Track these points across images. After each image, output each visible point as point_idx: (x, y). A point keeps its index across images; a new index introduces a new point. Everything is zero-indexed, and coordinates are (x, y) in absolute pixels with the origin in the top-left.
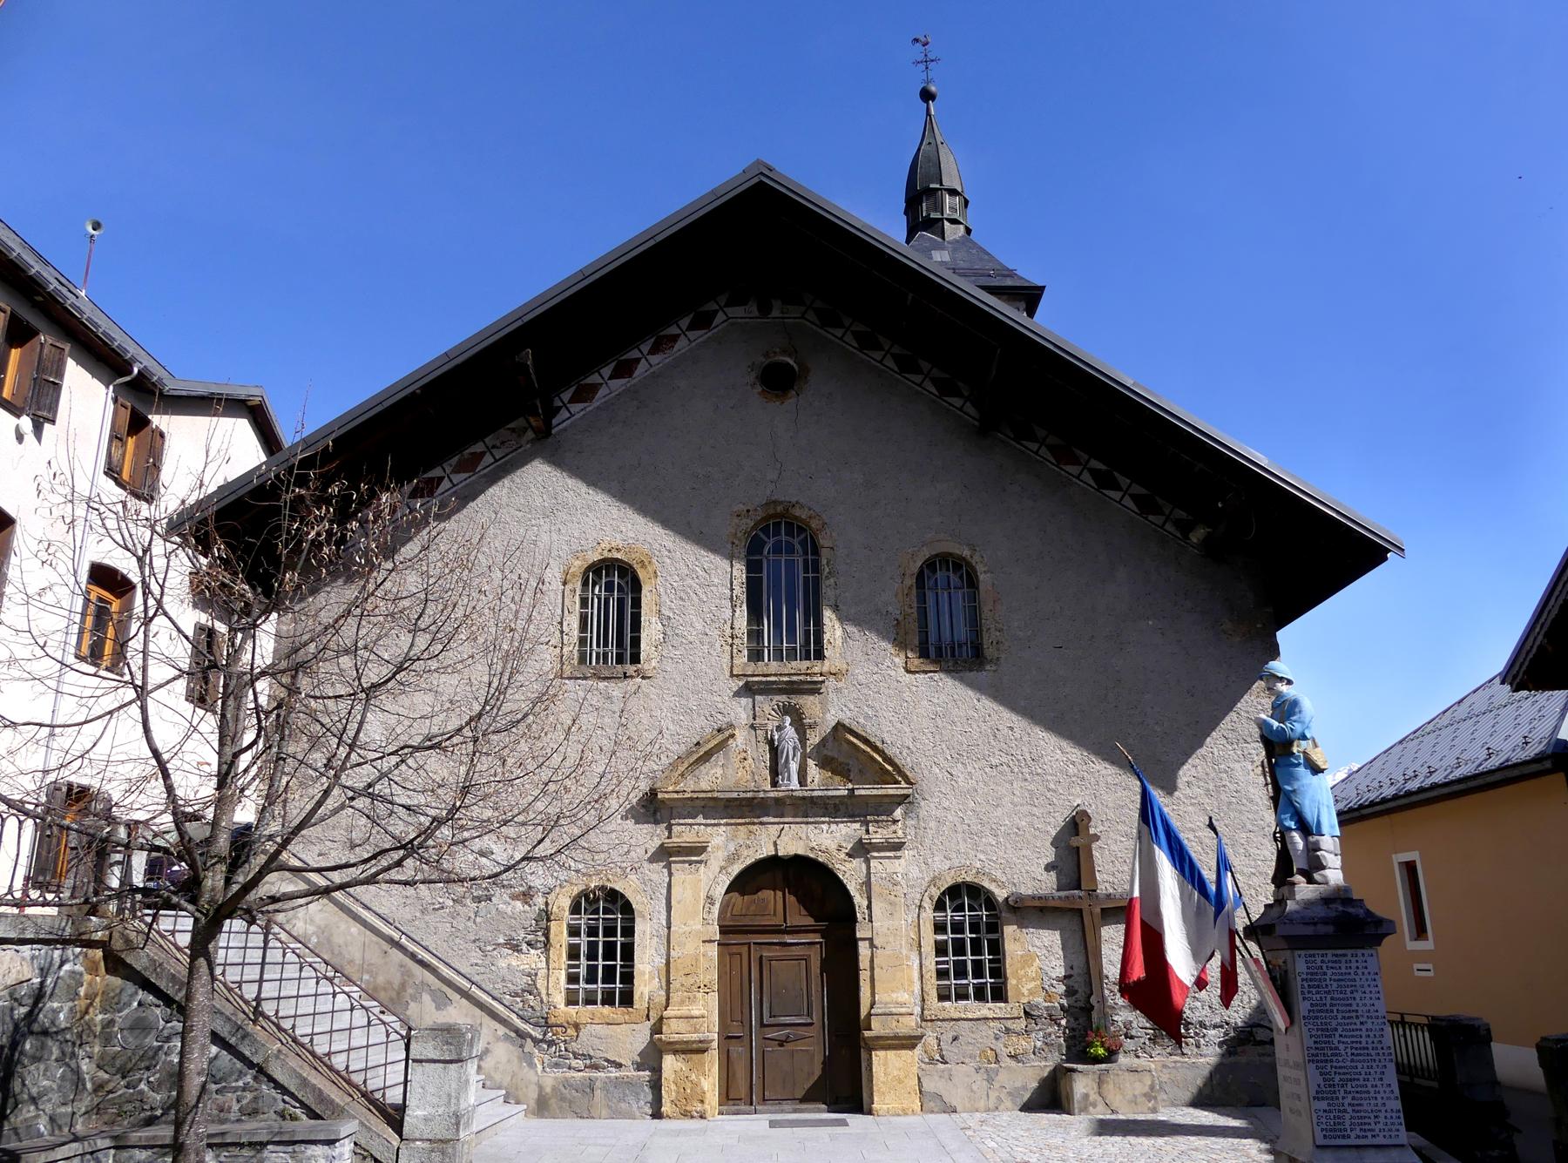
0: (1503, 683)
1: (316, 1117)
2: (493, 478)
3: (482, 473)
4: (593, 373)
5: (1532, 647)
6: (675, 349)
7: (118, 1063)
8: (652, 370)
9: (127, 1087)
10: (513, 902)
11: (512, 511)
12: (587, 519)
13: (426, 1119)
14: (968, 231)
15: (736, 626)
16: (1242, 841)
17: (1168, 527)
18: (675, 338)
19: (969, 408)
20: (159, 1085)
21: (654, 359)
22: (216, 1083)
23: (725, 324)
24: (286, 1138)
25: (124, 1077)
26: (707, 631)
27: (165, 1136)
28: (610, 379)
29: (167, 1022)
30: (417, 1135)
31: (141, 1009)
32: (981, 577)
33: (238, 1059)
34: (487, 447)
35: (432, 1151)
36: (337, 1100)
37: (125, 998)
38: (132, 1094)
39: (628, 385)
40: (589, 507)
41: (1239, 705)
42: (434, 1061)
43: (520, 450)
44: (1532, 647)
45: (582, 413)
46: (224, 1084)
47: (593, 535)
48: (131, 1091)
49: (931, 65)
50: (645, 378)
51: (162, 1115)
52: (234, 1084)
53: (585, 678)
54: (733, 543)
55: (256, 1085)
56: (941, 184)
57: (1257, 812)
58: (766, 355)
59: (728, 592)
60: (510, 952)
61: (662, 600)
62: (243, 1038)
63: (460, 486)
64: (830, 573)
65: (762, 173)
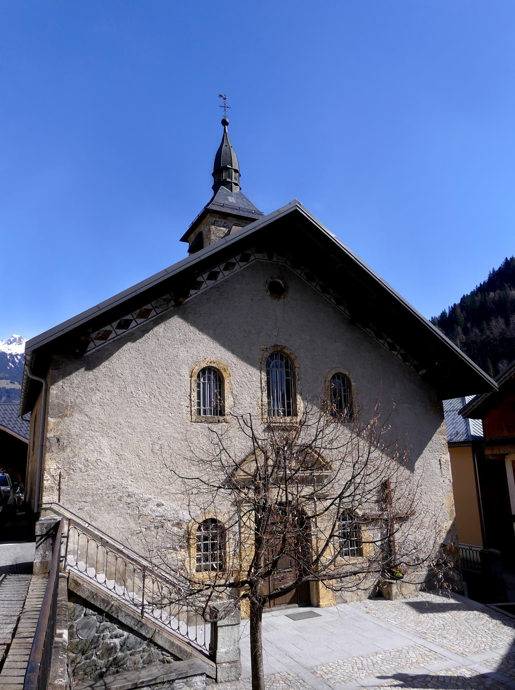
0: (459, 414)
1: (177, 659)
2: (157, 322)
3: (151, 319)
4: (199, 276)
5: (475, 405)
6: (234, 270)
7: (80, 647)
8: (225, 278)
9: (86, 659)
10: (173, 528)
11: (166, 340)
12: (199, 347)
13: (226, 653)
14: (240, 189)
15: (264, 400)
16: (434, 490)
17: (412, 367)
18: (234, 265)
19: (347, 311)
20: (102, 656)
21: (226, 273)
22: (129, 650)
23: (254, 261)
24: (184, 676)
25: (83, 654)
26: (252, 402)
27: (129, 685)
28: (207, 280)
29: (100, 623)
30: (223, 661)
31: (86, 617)
32: (353, 384)
33: (138, 637)
34: (153, 307)
35: (232, 667)
36: (188, 650)
37: (77, 613)
38: (89, 663)
39: (215, 284)
40: (200, 341)
41: (433, 438)
42: (228, 626)
43: (168, 310)
44: (475, 405)
45: (195, 295)
46: (133, 650)
47: (202, 354)
48: (88, 661)
49: (227, 109)
50: (222, 281)
51: (106, 671)
52: (138, 650)
53: (202, 422)
54: (261, 363)
55: (148, 648)
56: (232, 166)
57: (438, 479)
58: (272, 278)
59: (259, 384)
60: (173, 551)
61: (233, 387)
62: (141, 627)
63: (141, 325)
64: (298, 378)
65: (297, 206)
